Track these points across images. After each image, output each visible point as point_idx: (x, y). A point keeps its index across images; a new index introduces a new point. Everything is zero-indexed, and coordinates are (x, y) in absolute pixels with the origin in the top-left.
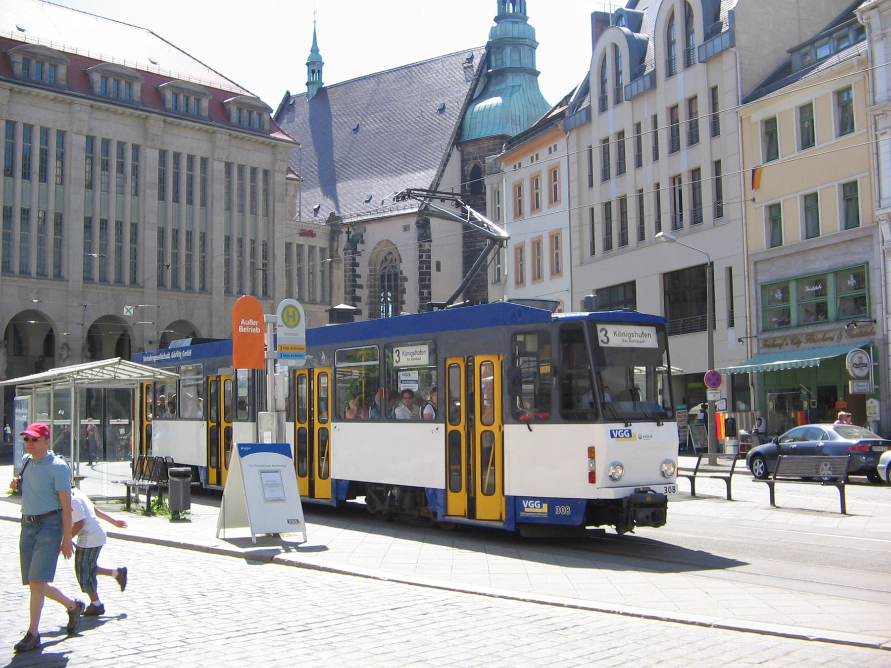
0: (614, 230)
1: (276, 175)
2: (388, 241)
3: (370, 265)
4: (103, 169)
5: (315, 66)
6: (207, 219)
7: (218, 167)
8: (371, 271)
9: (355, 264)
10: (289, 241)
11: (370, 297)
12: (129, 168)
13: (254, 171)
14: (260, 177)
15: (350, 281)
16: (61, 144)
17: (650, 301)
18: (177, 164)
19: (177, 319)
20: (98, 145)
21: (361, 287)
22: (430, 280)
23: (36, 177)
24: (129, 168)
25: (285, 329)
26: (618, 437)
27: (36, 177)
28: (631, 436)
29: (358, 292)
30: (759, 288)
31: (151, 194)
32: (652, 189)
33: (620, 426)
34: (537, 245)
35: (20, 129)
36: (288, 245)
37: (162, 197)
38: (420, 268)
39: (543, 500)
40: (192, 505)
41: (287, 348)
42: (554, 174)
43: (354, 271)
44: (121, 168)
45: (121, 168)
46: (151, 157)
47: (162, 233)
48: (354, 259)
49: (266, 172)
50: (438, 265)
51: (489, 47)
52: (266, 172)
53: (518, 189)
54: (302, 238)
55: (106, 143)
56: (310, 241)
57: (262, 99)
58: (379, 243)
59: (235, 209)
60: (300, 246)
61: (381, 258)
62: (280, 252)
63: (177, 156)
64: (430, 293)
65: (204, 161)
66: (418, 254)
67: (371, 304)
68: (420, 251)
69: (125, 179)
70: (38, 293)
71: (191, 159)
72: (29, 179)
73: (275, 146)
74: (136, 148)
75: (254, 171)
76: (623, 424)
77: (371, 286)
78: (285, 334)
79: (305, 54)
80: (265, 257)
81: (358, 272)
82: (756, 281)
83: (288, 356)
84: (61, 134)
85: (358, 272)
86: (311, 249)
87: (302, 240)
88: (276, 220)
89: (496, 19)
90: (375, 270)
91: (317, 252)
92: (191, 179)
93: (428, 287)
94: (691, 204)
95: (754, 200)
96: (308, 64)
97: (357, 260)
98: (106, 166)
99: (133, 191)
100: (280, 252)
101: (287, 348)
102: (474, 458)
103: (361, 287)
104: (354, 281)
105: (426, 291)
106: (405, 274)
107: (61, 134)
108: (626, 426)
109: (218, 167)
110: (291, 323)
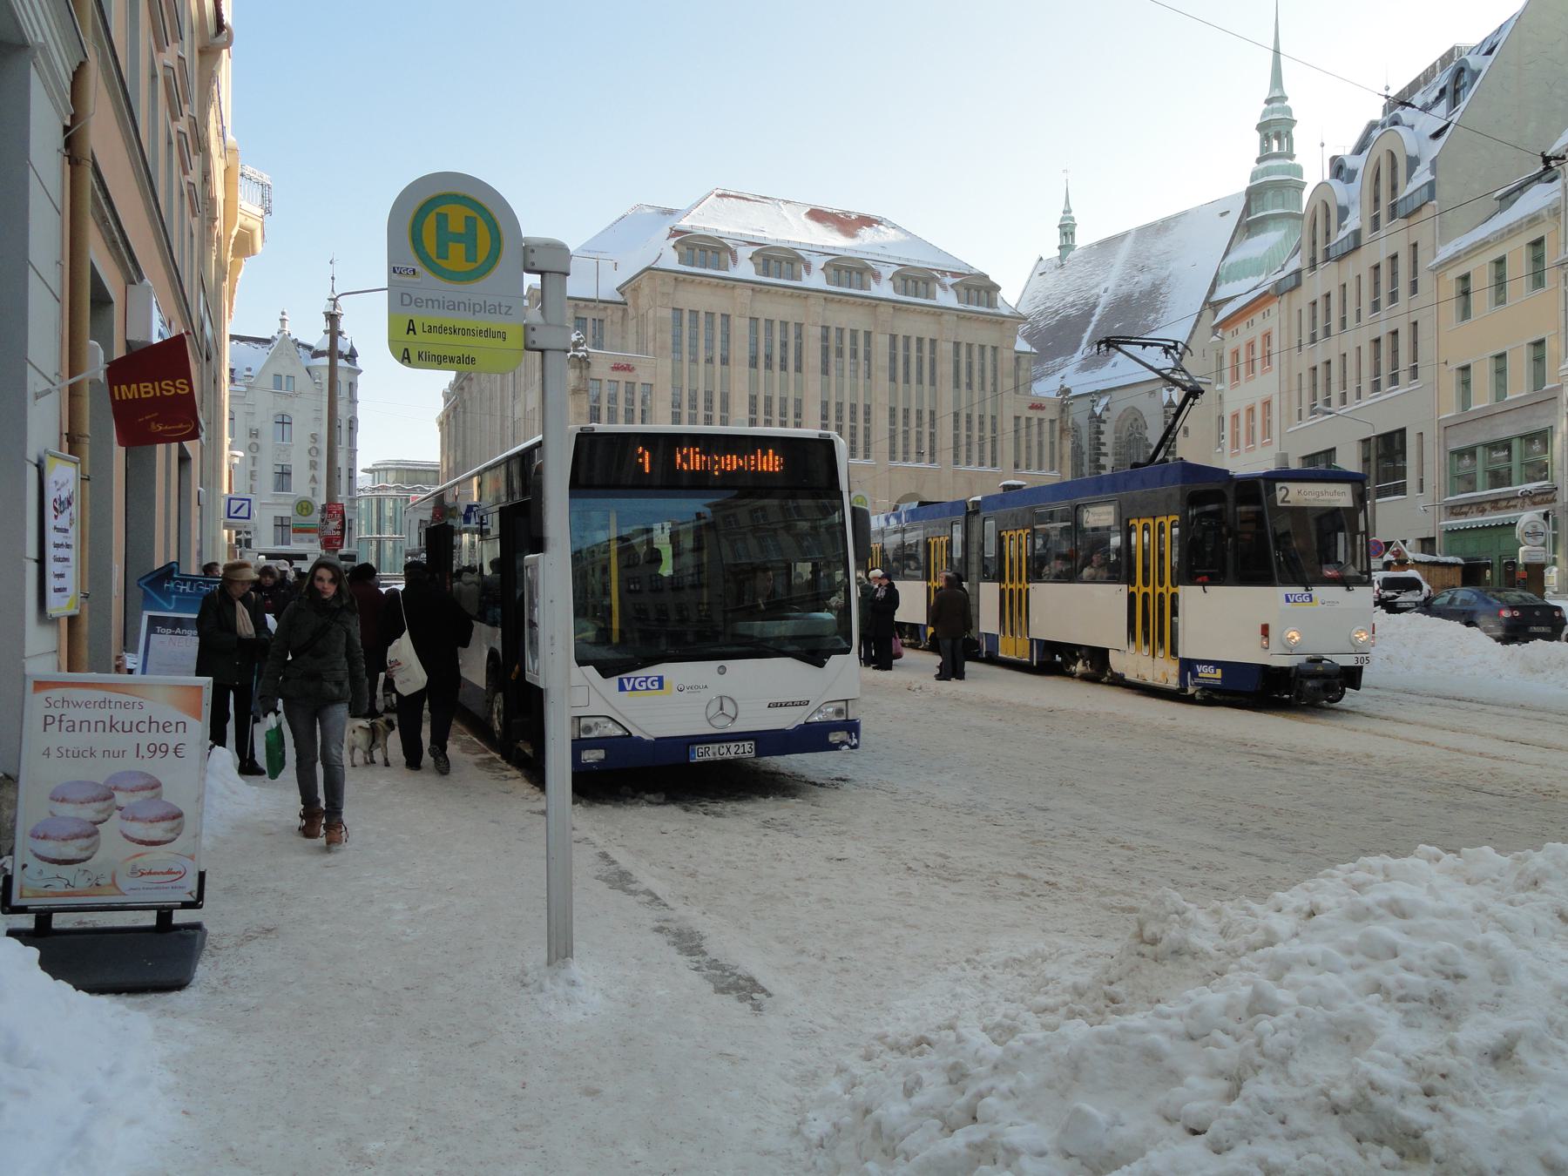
0: (1321, 389)
5: (1067, 230)
6: (934, 397)
7: (945, 349)
9: (1100, 433)
12: (861, 354)
13: (982, 347)
16: (799, 336)
17: (1349, 460)
18: (907, 347)
21: (1105, 455)
23: (777, 368)
24: (861, 354)
27: (777, 368)
29: (1103, 460)
31: (882, 377)
32: (1354, 352)
33: (1300, 590)
34: (1251, 410)
35: (762, 323)
36: (1017, 418)
37: (893, 379)
39: (1216, 664)
42: (1267, 337)
44: (854, 354)
45: (854, 354)
46: (881, 343)
47: (893, 411)
49: (995, 349)
51: (1250, 193)
52: (995, 349)
53: (1236, 353)
55: (840, 331)
56: (1040, 414)
57: (992, 278)
59: (963, 386)
60: (1028, 419)
62: (1008, 426)
69: (857, 364)
71: (920, 340)
75: (982, 347)
79: (1056, 217)
80: (994, 430)
84: (799, 326)
86: (1041, 421)
87: (1031, 413)
89: (1259, 161)
91: (1046, 425)
92: (920, 360)
94: (1392, 360)
96: (1260, 127)
98: (840, 353)
100: (1008, 426)
103: (1105, 455)
107: (799, 326)
109: (945, 349)
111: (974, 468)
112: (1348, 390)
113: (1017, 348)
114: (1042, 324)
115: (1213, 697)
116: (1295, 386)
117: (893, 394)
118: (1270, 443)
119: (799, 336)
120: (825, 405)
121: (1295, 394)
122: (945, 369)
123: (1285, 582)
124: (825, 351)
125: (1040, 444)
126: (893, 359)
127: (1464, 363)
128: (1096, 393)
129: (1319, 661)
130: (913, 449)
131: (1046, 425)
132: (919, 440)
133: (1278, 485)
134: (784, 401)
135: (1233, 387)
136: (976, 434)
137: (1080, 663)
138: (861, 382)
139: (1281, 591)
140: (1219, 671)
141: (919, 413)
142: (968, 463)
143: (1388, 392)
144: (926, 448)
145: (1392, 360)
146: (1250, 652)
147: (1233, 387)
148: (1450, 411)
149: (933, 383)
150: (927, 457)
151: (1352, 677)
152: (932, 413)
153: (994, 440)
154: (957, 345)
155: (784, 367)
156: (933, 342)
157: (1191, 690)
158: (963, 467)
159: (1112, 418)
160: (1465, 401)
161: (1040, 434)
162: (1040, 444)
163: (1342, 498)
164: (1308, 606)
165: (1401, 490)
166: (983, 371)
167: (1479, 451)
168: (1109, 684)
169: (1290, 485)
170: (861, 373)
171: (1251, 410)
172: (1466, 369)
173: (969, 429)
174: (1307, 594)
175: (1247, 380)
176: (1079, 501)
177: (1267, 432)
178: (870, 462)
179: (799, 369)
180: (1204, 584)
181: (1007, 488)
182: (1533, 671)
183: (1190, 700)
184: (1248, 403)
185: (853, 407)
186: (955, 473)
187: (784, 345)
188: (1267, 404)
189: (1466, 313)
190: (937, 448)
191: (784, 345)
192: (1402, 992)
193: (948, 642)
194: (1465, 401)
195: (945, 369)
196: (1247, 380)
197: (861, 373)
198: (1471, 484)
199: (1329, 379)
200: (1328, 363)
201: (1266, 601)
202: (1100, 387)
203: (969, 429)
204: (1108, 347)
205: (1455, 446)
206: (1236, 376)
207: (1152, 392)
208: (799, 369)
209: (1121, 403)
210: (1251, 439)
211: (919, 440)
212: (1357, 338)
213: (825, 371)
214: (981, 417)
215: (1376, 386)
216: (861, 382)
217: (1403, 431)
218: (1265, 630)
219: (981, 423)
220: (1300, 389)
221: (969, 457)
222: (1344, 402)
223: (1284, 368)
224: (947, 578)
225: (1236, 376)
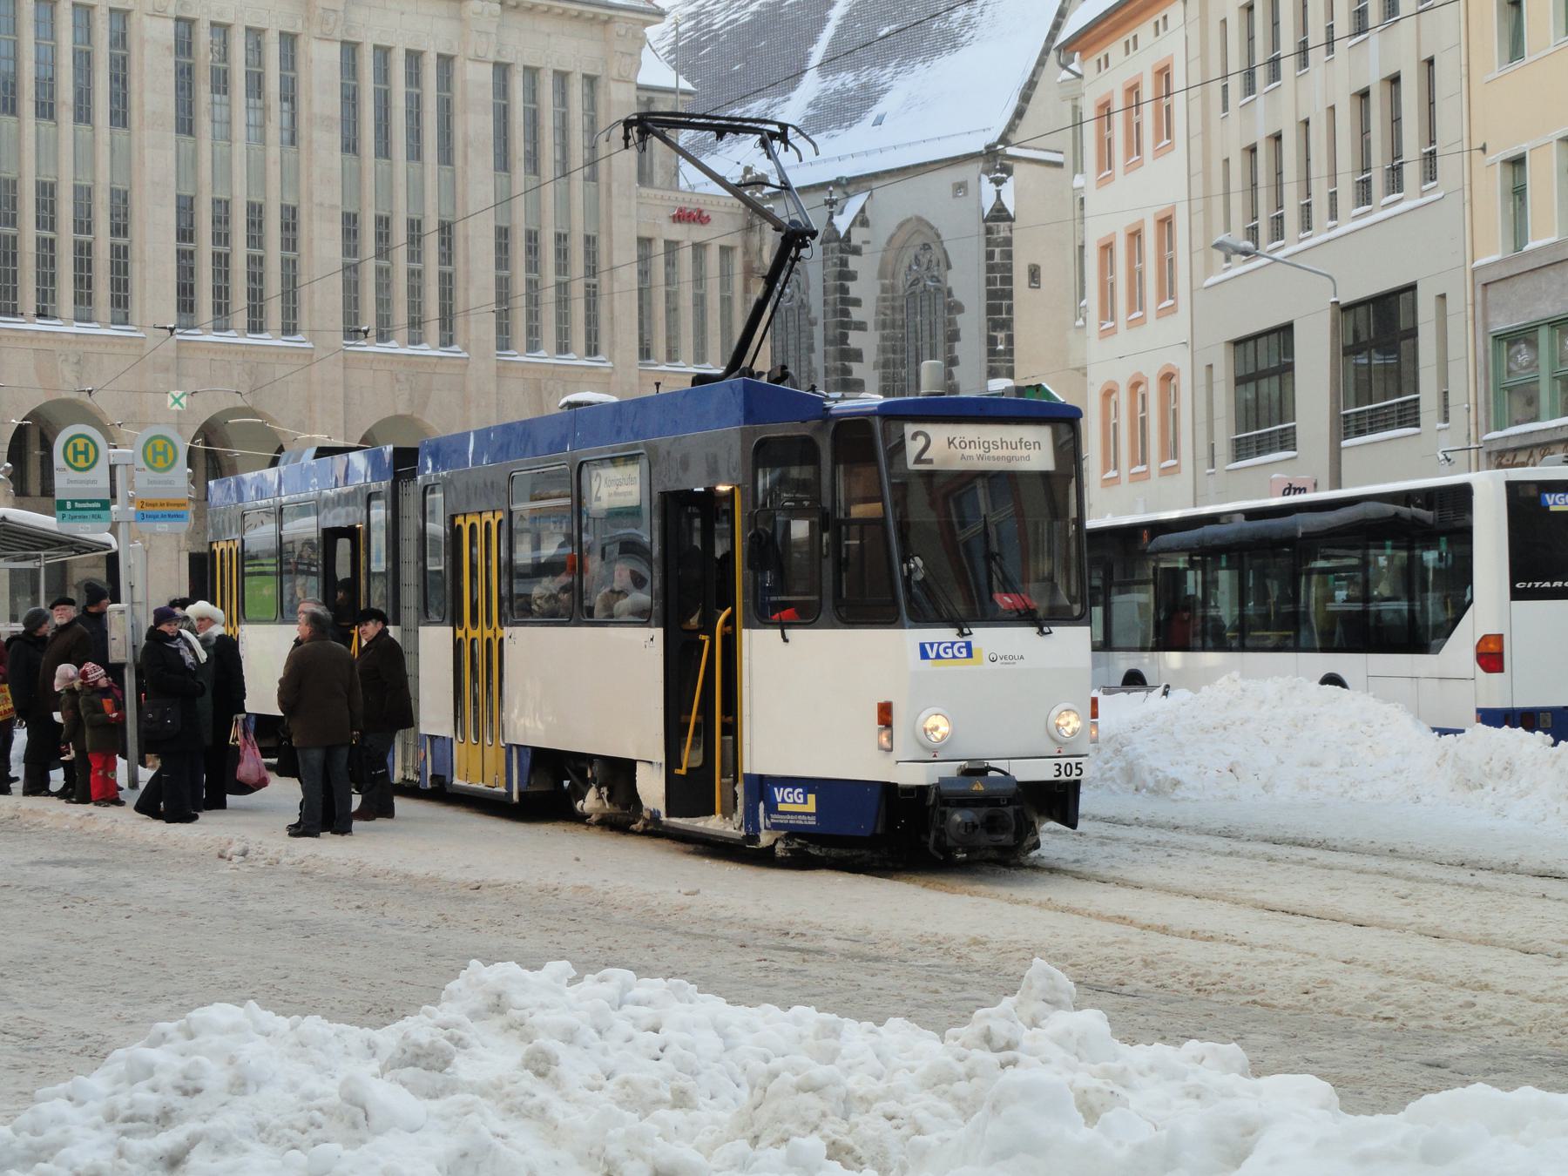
0: (1266, 199)
1: (613, 85)
2: (920, 220)
3: (882, 274)
4: (215, 89)
7: (475, 78)
8: (884, 289)
9: (846, 275)
10: (646, 234)
11: (883, 350)
12: (273, 85)
13: (562, 77)
14: (576, 91)
15: (835, 315)
16: (120, 40)
18: (383, 74)
19: (391, 413)
20: (203, 37)
21: (861, 326)
22: (1010, 309)
23: (66, 114)
24: (273, 85)
25: (149, 473)
26: (938, 656)
27: (66, 114)
28: (970, 655)
29: (855, 339)
30: (1490, 340)
31: (324, 143)
33: (947, 634)
34: (1135, 235)
36: (645, 242)
37: (350, 146)
38: (989, 282)
40: (229, 798)
41: (153, 505)
42: (1164, 73)
43: (844, 290)
44: (256, 85)
45: (256, 85)
47: (351, 225)
48: (844, 263)
49: (591, 81)
50: (1034, 274)
52: (591, 81)
54: (678, 226)
56: (698, 233)
58: (901, 226)
60: (672, 246)
61: (908, 258)
62: (621, 256)
63: (383, 53)
64: (1010, 340)
65: (446, 61)
66: (983, 249)
67: (885, 365)
68: (989, 242)
69: (265, 109)
70: (78, 363)
71: (414, 57)
72: (51, 117)
73: (608, 21)
74: (289, 40)
75: (562, 77)
76: (955, 631)
77: (884, 325)
78: (150, 482)
80: (592, 270)
81: (853, 294)
82: (1486, 326)
83: (155, 517)
85: (853, 294)
87: (678, 232)
88: (615, 186)
90: (893, 288)
91: (713, 258)
93: (1007, 325)
95: (1484, 149)
97: (852, 267)
98: (221, 83)
99: (287, 136)
100: (621, 256)
101: (153, 505)
102: (701, 699)
103: (861, 326)
104: (846, 313)
105: (1001, 335)
106: (958, 296)
108: (962, 634)
109: (475, 78)
110: (160, 462)
111: (546, 356)
112: (1314, 199)
113: (644, 78)
114: (719, 21)
115: (812, 850)
116: (1218, 187)
117: (351, 182)
118: (1172, 310)
119: (120, 40)
120: (186, 207)
121: (1218, 203)
122: (476, 125)
123: (922, 617)
124: (185, 77)
125: (700, 302)
126: (350, 99)
127: (1512, 152)
128: (837, 183)
129: (983, 772)
130: (401, 314)
131: (713, 258)
132: (415, 291)
133: (910, 429)
134: (84, 196)
135: (1103, 182)
136: (549, 276)
137: (591, 795)
138: (274, 152)
139: (910, 638)
140: (812, 798)
141: (415, 227)
142: (533, 347)
143: (1384, 207)
144: (432, 308)
145: (1392, 140)
146: (860, 759)
147: (1103, 182)
148: (1492, 252)
149: (446, 155)
150: (433, 328)
151: (1058, 800)
152: (446, 229)
153: (592, 294)
154: (502, 70)
155: (83, 114)
156: (446, 61)
157: (765, 839)
158: (519, 356)
159: (874, 242)
160: (1519, 232)
161: (699, 279)
162: (700, 302)
163: (1034, 453)
164: (963, 666)
165: (1408, 415)
166: (563, 129)
167: (1544, 334)
168: (645, 833)
169: (929, 429)
170: (274, 133)
171: (1135, 235)
172: (1517, 163)
173: (533, 265)
174: (961, 641)
175: (1128, 168)
176: (584, 454)
177: (1167, 287)
178: (299, 341)
179: (120, 117)
180: (783, 626)
181: (571, 405)
182: (1470, 785)
183: (766, 859)
184: (1130, 220)
185: (256, 214)
186: (502, 370)
187: (84, 61)
188: (1166, 223)
189: (1516, 49)
190: (459, 306)
191: (84, 61)
192: (128, 1112)
193: (316, 756)
194: (1519, 232)
195: (476, 125)
196: (1128, 168)
197: (274, 133)
198: (1531, 407)
199: (1279, 174)
200: (1278, 138)
201: (884, 656)
202: (849, 170)
203: (533, 265)
204: (644, 133)
205: (1501, 324)
206: (1106, 159)
207: (960, 187)
208: (120, 117)
209: (894, 205)
210: (1136, 300)
211: (415, 291)
212: (1325, 86)
213: (186, 125)
214: (561, 238)
215: (1364, 193)
216: (274, 152)
217: (1412, 288)
218: (885, 714)
219: (562, 254)
220: (1227, 193)
221: (533, 332)
222: (1307, 224)
223: (1196, 144)
224: (314, 619)
225: (1106, 159)
